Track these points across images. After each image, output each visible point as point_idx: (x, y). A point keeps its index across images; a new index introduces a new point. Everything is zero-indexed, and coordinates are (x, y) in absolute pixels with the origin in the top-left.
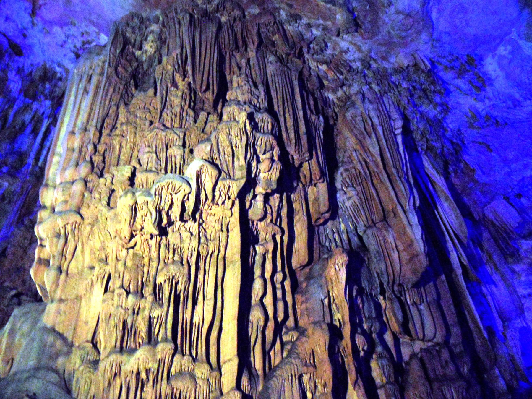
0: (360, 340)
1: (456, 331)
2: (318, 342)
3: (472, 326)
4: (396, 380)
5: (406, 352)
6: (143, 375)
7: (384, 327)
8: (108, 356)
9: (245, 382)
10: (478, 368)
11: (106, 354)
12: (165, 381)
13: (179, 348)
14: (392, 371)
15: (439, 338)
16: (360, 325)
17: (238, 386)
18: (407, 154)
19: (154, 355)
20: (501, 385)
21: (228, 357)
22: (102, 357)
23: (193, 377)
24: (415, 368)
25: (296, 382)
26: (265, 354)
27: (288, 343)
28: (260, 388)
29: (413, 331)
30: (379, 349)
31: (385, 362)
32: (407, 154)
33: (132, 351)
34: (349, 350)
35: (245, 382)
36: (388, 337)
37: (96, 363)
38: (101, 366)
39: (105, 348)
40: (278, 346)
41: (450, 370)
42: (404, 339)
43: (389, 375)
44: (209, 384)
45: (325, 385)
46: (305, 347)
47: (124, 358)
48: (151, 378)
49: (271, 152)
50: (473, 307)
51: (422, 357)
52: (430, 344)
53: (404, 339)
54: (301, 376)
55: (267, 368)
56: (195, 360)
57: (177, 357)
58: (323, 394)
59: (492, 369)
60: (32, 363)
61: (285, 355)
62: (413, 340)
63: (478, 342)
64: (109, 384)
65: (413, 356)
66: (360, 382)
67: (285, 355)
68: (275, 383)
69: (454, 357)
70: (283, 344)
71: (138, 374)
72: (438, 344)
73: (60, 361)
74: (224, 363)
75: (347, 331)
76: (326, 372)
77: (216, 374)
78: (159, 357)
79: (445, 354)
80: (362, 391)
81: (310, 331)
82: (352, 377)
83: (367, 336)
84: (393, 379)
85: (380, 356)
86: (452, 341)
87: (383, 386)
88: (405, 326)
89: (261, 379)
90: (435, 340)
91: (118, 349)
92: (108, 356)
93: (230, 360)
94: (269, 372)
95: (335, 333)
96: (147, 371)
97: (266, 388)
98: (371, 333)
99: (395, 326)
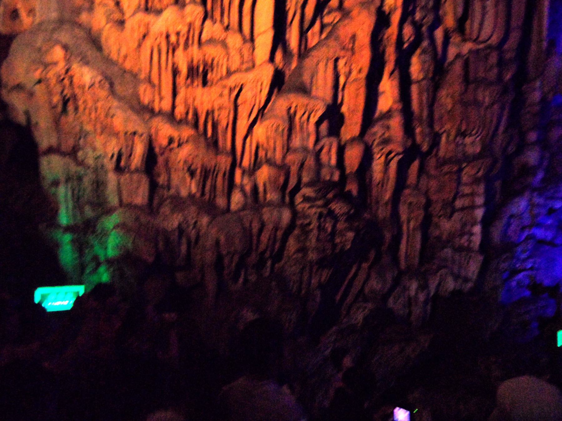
0: (408, 30)
1: (514, 38)
2: (362, 25)
3: (535, 27)
4: (433, 79)
5: (452, 52)
6: (173, 39)
7: (438, 22)
8: (134, 14)
9: (279, 56)
10: (522, 78)
11: (132, 12)
12: (196, 46)
13: (210, 14)
14: (431, 68)
15: (494, 40)
16: (413, 12)
17: (272, 59)
18: (504, 119)
19: (183, 17)
20: (536, 96)
21: (263, 29)
22: (127, 15)
23: (224, 44)
24: (458, 68)
25: (331, 65)
26: (303, 33)
27: (329, 24)
28: (294, 65)
29: (468, 31)
30: (425, 44)
31: (427, 58)
32: (504, 119)
33: (159, 12)
34: (394, 37)
35: (279, 56)
36: (439, 34)
37: (121, 23)
38: (128, 25)
39: (129, 6)
40: (317, 26)
41: (493, 74)
42: (455, 39)
43: (428, 71)
44: (242, 57)
45: (360, 71)
46: (346, 31)
47: (150, 18)
48: (182, 41)
49: (343, 143)
50: (545, 22)
51: (468, 58)
52: (481, 46)
53: (455, 39)
54: (336, 60)
55: (303, 47)
56: (227, 28)
57: (208, 23)
58: (355, 80)
59: (535, 79)
60: (54, 15)
61: (324, 36)
62: (464, 40)
63: (534, 47)
64: (139, 46)
65: (458, 56)
66: (396, 73)
67: (324, 36)
68: (309, 62)
69: (501, 63)
70: (323, 27)
71: (168, 37)
72: (490, 47)
73: (84, 17)
74: (259, 35)
75: (396, 18)
76: (364, 58)
77: (248, 45)
78: (189, 20)
79: (493, 59)
80: (396, 83)
81: (355, 12)
82: (389, 67)
83: (417, 26)
84: (430, 75)
85: (424, 52)
86: (506, 47)
87: (418, 82)
88: (461, 22)
89: (295, 59)
90: (489, 42)
91: (143, 6)
92: (134, 14)
93: (264, 32)
94: (304, 52)
95: (382, 20)
96: (178, 34)
97: (299, 67)
98: (421, 26)
99: (450, 21)
